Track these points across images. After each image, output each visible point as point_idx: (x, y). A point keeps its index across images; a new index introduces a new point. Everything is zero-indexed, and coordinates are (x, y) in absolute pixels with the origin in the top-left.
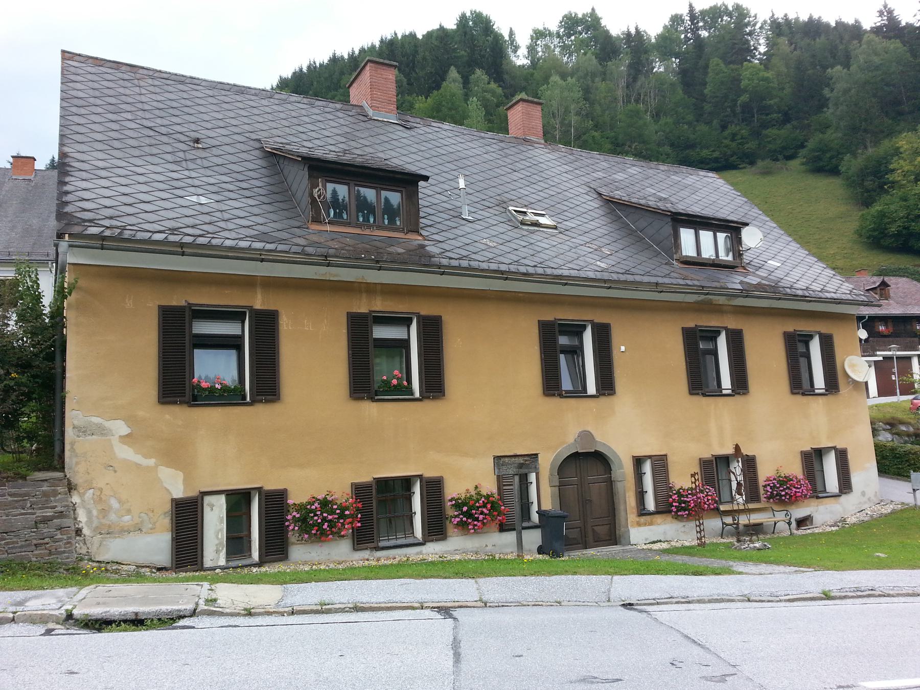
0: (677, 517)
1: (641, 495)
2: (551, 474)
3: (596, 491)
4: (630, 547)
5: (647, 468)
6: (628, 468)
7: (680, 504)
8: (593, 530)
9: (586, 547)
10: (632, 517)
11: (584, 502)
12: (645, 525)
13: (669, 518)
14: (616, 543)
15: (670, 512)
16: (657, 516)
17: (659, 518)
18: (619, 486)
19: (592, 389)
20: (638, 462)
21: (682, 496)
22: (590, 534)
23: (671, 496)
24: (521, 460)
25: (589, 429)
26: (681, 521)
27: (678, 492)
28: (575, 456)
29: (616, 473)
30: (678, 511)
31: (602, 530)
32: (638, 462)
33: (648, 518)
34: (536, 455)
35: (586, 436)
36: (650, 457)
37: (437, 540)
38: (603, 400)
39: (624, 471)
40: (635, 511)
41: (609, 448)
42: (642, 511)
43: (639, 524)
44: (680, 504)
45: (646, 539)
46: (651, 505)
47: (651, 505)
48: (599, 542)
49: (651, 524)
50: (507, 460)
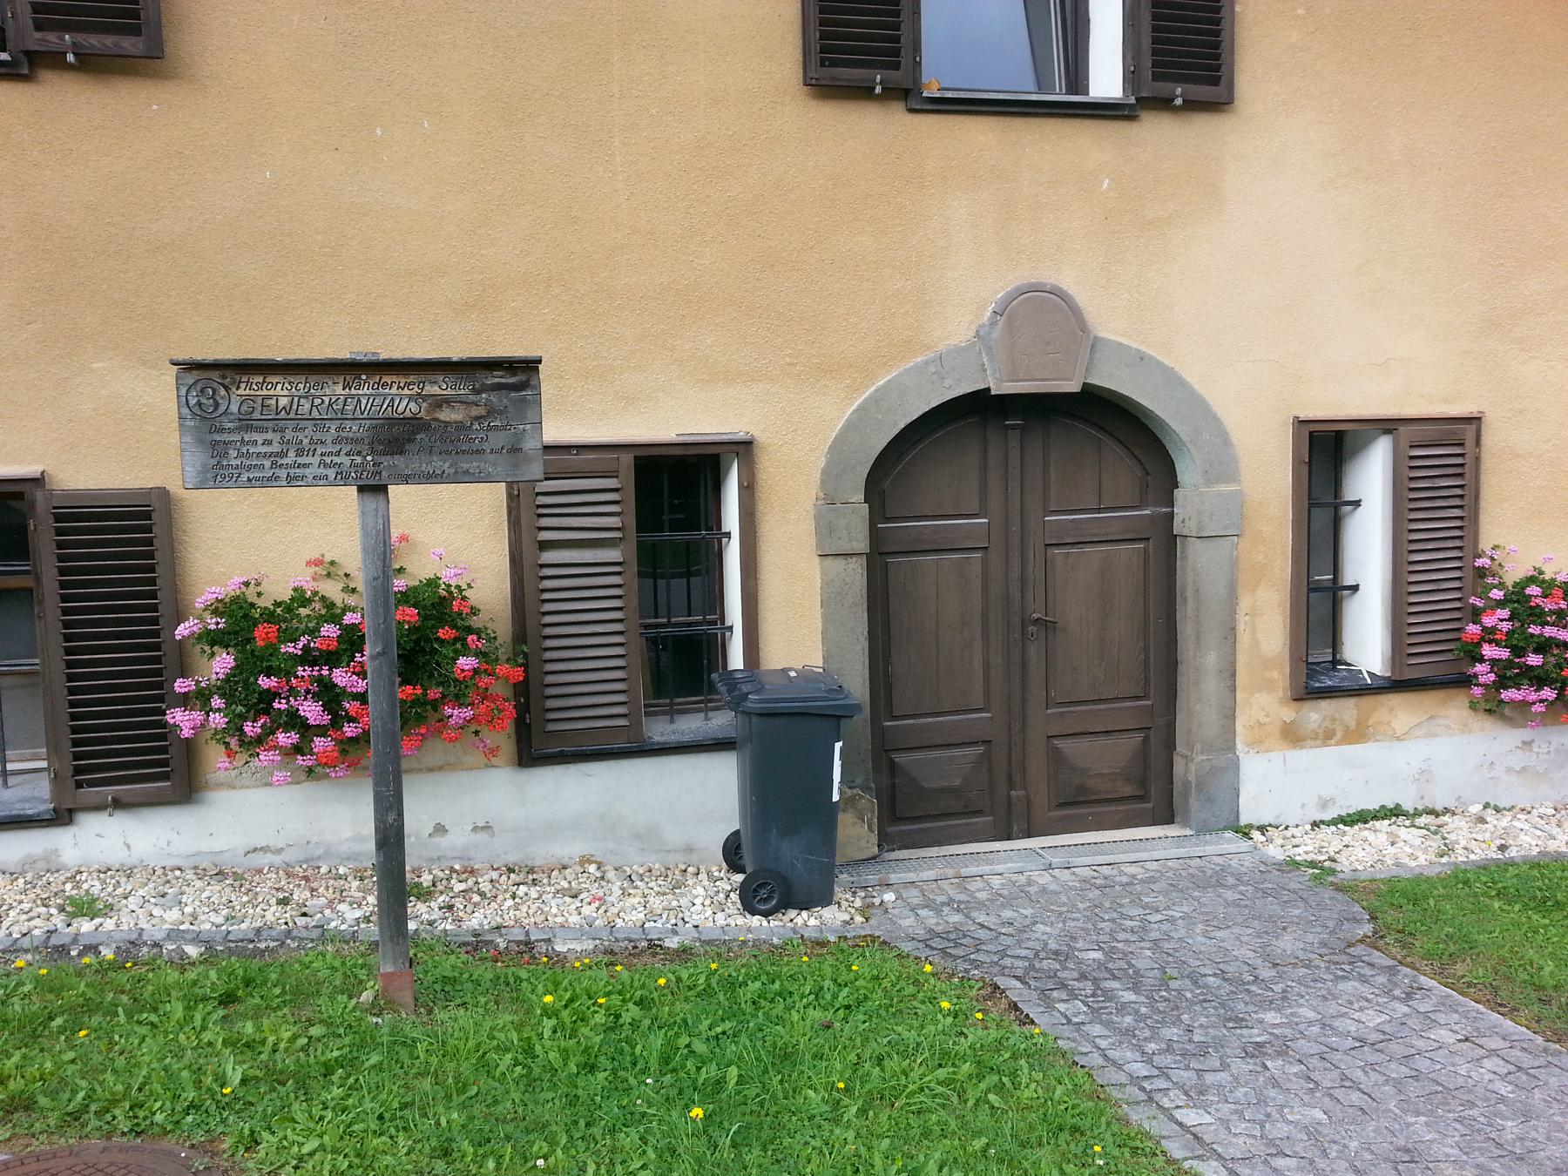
0: (1493, 708)
1: (1320, 600)
2: (830, 500)
3: (1086, 586)
4: (1230, 843)
5: (1372, 478)
6: (1268, 477)
7: (1518, 651)
8: (1056, 757)
9: (1009, 837)
10: (1263, 701)
11: (1027, 628)
12: (1326, 737)
13: (1453, 709)
14: (1169, 820)
15: (1464, 682)
16: (1394, 700)
17: (1401, 711)
18: (1200, 565)
19: (1106, 76)
20: (1326, 450)
21: (1537, 615)
22: (1037, 766)
23: (1476, 615)
24: (401, 398)
25: (1067, 280)
26: (1510, 721)
27: (1517, 599)
28: (974, 412)
29: (1193, 501)
30: (1502, 683)
31: (1104, 758)
32: (1326, 450)
33: (1346, 709)
34: (529, 366)
35: (1041, 310)
36: (1387, 426)
37: (118, 804)
38: (1159, 134)
39: (1241, 491)
40: (1280, 676)
41: (1172, 378)
42: (1319, 674)
43: (1292, 736)
44: (1518, 651)
45: (1324, 804)
46: (1367, 642)
47: (1367, 642)
48: (1080, 806)
49: (1358, 735)
50: (281, 392)
